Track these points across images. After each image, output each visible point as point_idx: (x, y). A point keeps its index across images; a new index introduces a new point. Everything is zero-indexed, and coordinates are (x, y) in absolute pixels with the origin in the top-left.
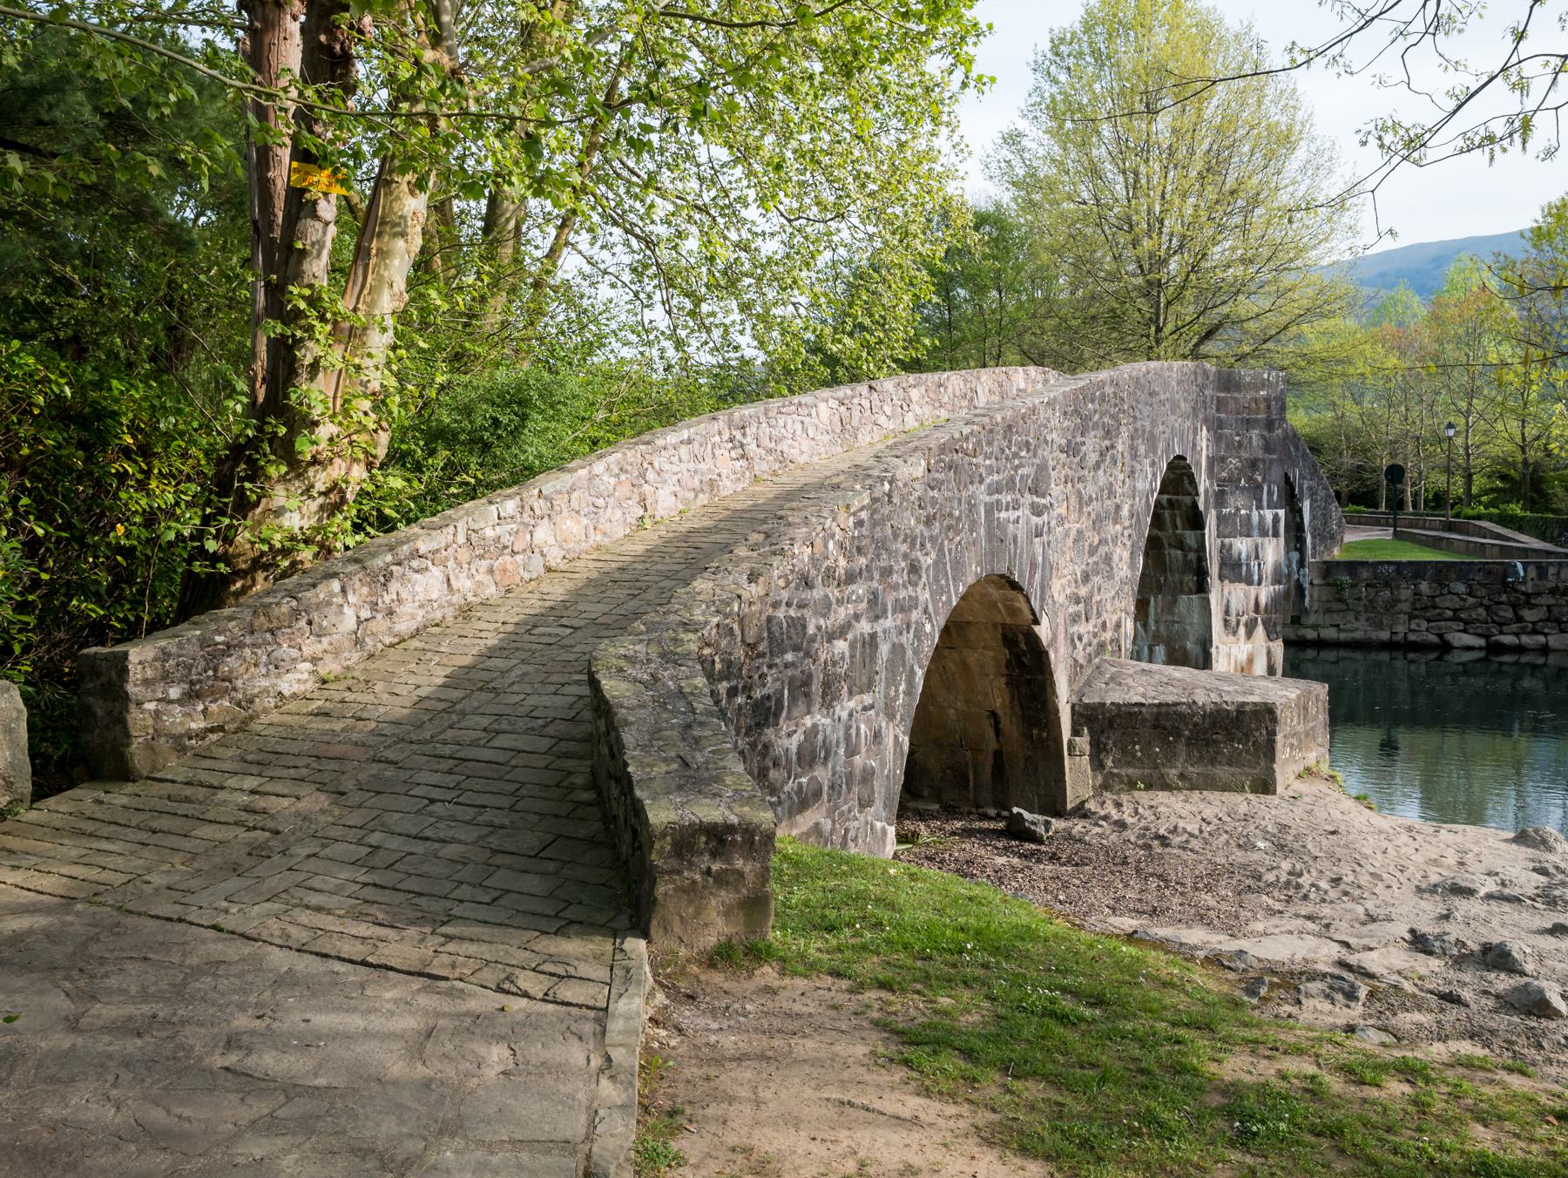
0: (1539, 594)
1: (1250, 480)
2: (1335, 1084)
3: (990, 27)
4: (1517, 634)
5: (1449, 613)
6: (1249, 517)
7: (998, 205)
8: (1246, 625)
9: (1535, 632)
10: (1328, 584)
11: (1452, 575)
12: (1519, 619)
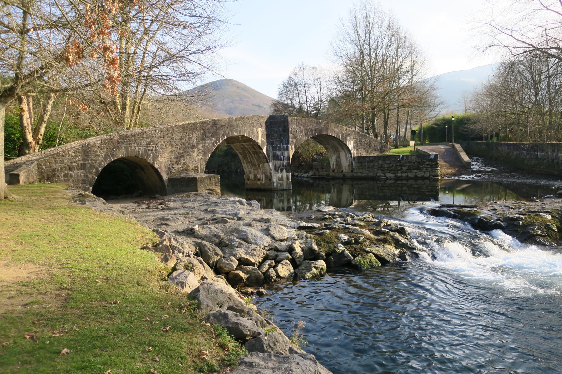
0: (406, 163)
4: (401, 173)
5: (386, 168)
6: (280, 147)
8: (280, 169)
9: (405, 172)
10: (358, 162)
12: (402, 169)
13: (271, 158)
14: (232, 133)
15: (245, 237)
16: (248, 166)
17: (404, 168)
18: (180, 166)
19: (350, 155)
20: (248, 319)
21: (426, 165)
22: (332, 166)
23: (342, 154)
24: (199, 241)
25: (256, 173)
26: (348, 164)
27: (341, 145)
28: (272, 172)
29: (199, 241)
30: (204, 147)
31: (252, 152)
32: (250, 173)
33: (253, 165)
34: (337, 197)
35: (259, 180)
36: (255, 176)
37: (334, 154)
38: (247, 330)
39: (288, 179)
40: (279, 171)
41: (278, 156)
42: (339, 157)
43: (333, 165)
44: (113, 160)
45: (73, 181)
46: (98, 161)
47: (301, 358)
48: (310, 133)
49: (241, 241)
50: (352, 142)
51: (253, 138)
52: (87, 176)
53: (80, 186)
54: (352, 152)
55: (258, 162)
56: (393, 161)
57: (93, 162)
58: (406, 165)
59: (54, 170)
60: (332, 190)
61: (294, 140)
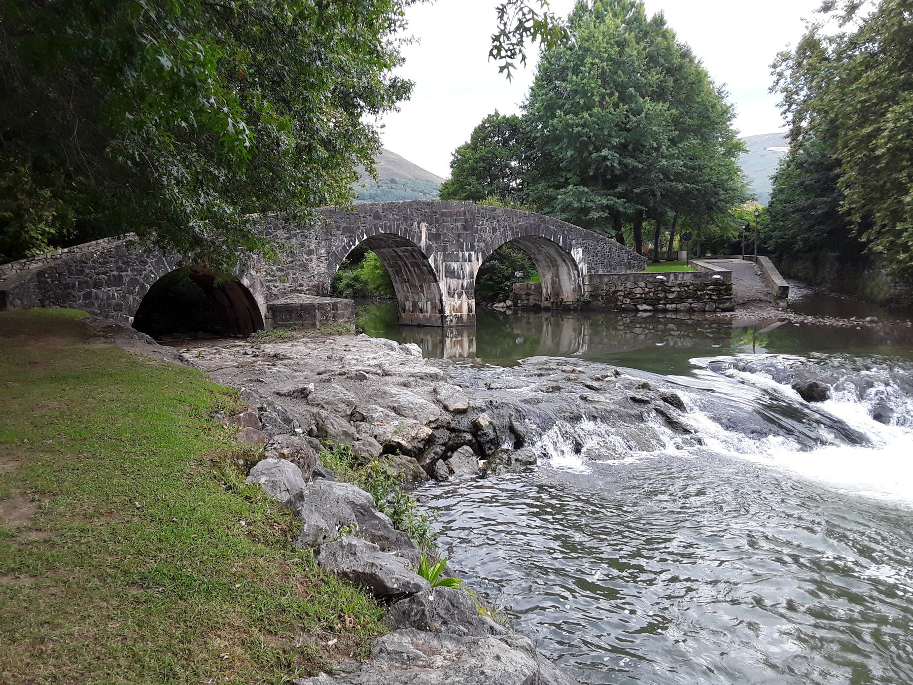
1: (458, 241)
2: (295, 343)
3: (404, 60)
5: (638, 296)
6: (458, 254)
7: (695, 57)
9: (672, 303)
11: (640, 279)
13: (442, 274)
14: (377, 230)
15: (396, 405)
16: (403, 288)
17: (671, 296)
18: (287, 285)
19: (576, 272)
20: (397, 555)
21: (710, 290)
22: (544, 291)
23: (563, 270)
24: (315, 410)
25: (416, 300)
26: (572, 287)
27: (561, 255)
28: (444, 298)
29: (315, 410)
30: (328, 253)
31: (410, 263)
32: (407, 299)
33: (412, 286)
34: (553, 341)
35: (421, 311)
36: (415, 305)
37: (549, 270)
38: (393, 580)
39: (470, 310)
40: (456, 296)
41: (454, 272)
42: (557, 276)
43: (547, 289)
44: (170, 271)
45: (99, 307)
46: (144, 272)
47: (503, 645)
48: (509, 233)
49: (386, 411)
50: (580, 251)
51: (413, 238)
52: (124, 297)
53: (111, 314)
54: (580, 266)
55: (419, 281)
56: (651, 283)
57: (135, 273)
58: (673, 289)
59: (67, 286)
60: (545, 328)
61: (482, 245)
